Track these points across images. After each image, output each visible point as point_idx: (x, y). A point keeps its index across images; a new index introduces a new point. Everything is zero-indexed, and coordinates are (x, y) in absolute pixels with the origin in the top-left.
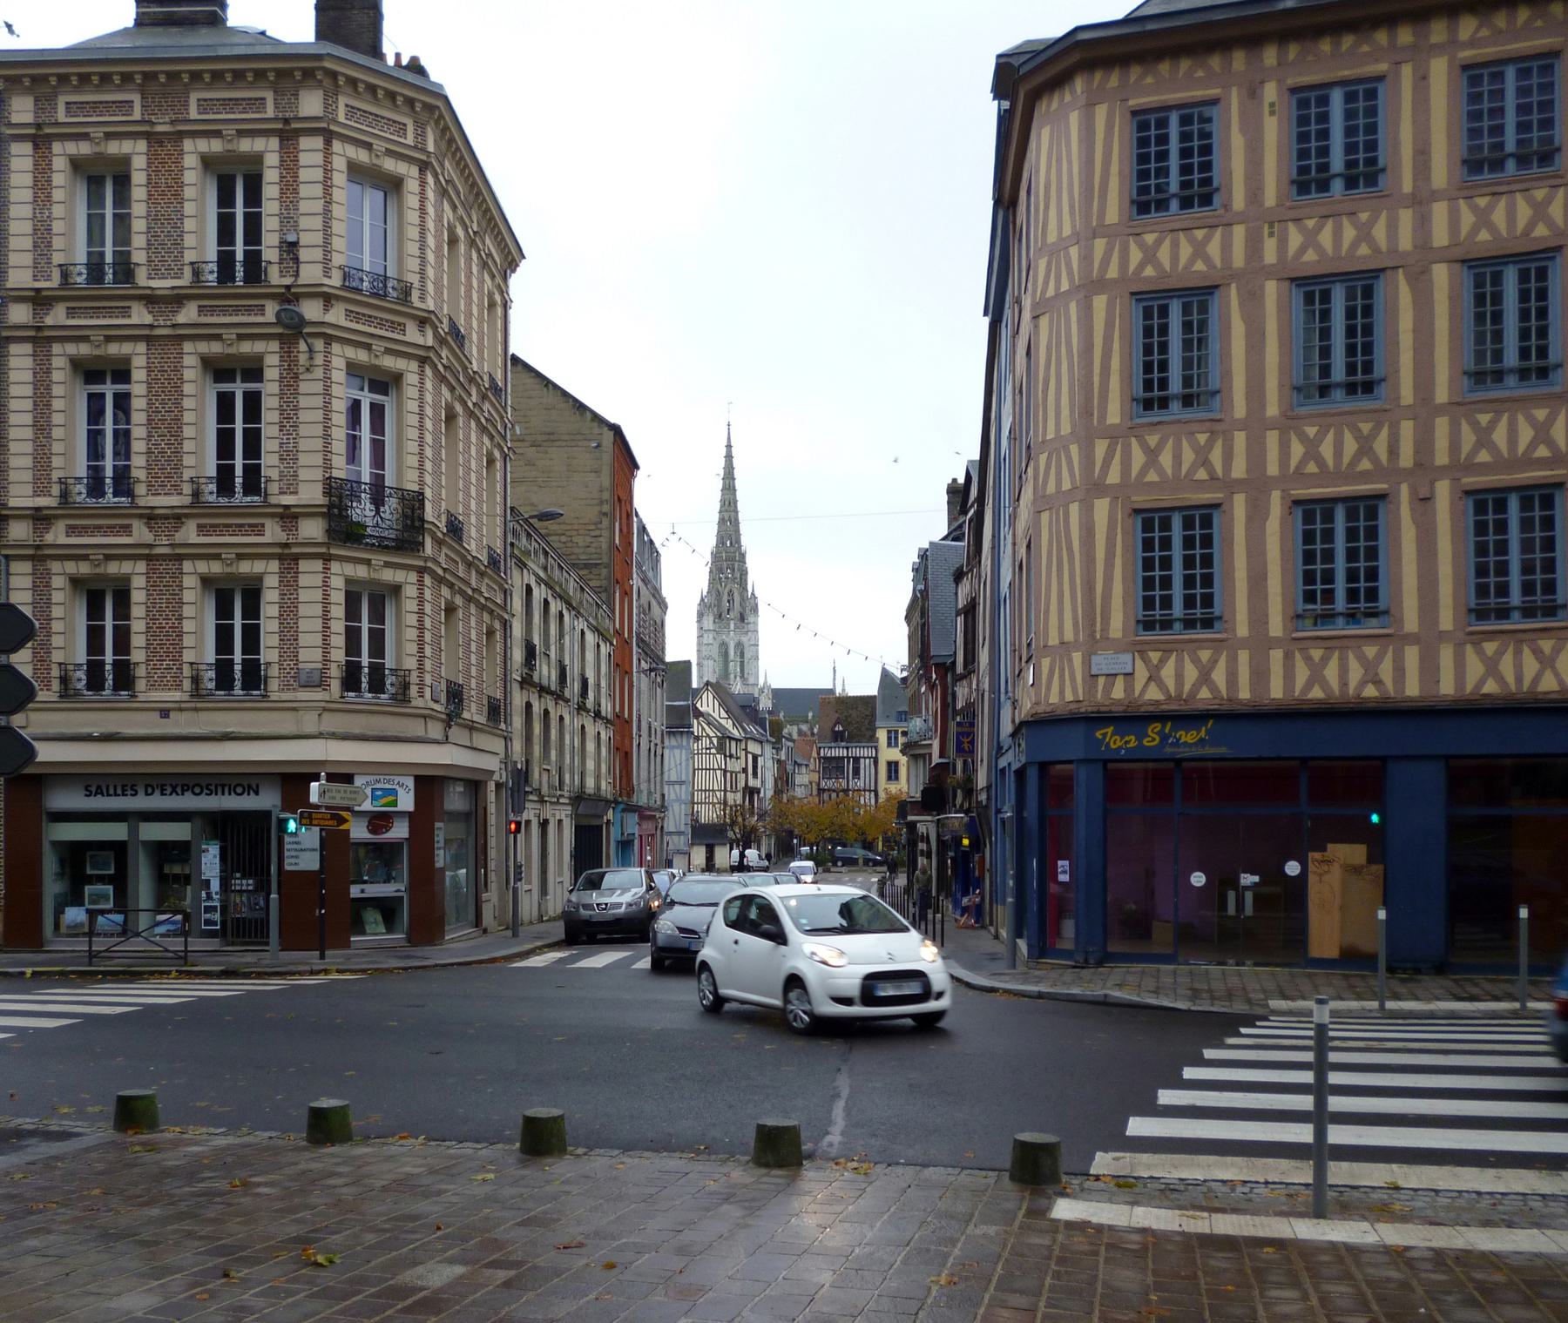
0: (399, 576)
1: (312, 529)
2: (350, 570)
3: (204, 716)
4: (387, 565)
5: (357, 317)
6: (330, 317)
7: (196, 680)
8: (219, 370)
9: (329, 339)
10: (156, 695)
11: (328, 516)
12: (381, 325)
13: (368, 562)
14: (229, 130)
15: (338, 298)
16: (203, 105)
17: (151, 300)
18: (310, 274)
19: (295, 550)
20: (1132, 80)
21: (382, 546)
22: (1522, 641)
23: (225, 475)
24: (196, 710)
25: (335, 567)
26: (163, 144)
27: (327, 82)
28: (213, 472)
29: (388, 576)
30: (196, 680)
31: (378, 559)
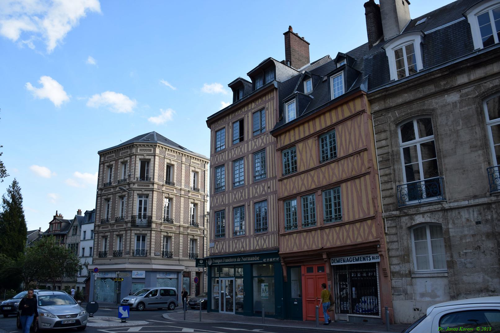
0: (146, 232)
1: (129, 225)
2: (136, 232)
3: (115, 260)
4: (143, 230)
5: (140, 185)
6: (134, 187)
7: (133, 253)
8: (140, 196)
9: (134, 191)
10: (109, 257)
11: (131, 222)
12: (145, 186)
13: (139, 230)
14: (145, 155)
15: (136, 183)
16: (141, 150)
17: (113, 187)
18: (132, 180)
19: (127, 229)
20: (230, 118)
21: (142, 227)
22: (261, 236)
23: (140, 214)
24: (114, 259)
25: (133, 232)
26: (116, 161)
27: (136, 146)
28: (138, 215)
29: (144, 232)
30: (133, 253)
31: (141, 229)
